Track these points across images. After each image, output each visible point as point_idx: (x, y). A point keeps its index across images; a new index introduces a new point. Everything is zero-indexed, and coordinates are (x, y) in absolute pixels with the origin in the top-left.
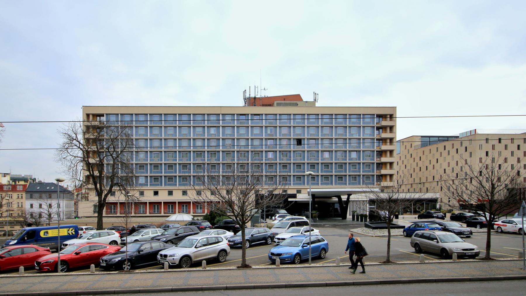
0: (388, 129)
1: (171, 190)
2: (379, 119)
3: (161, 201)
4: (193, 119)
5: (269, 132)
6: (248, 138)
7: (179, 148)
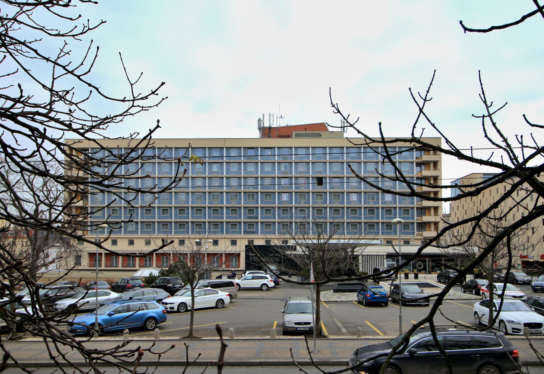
0: (432, 166)
2: (421, 153)
4: (312, 152)
5: (283, 169)
6: (256, 176)
7: (209, 189)
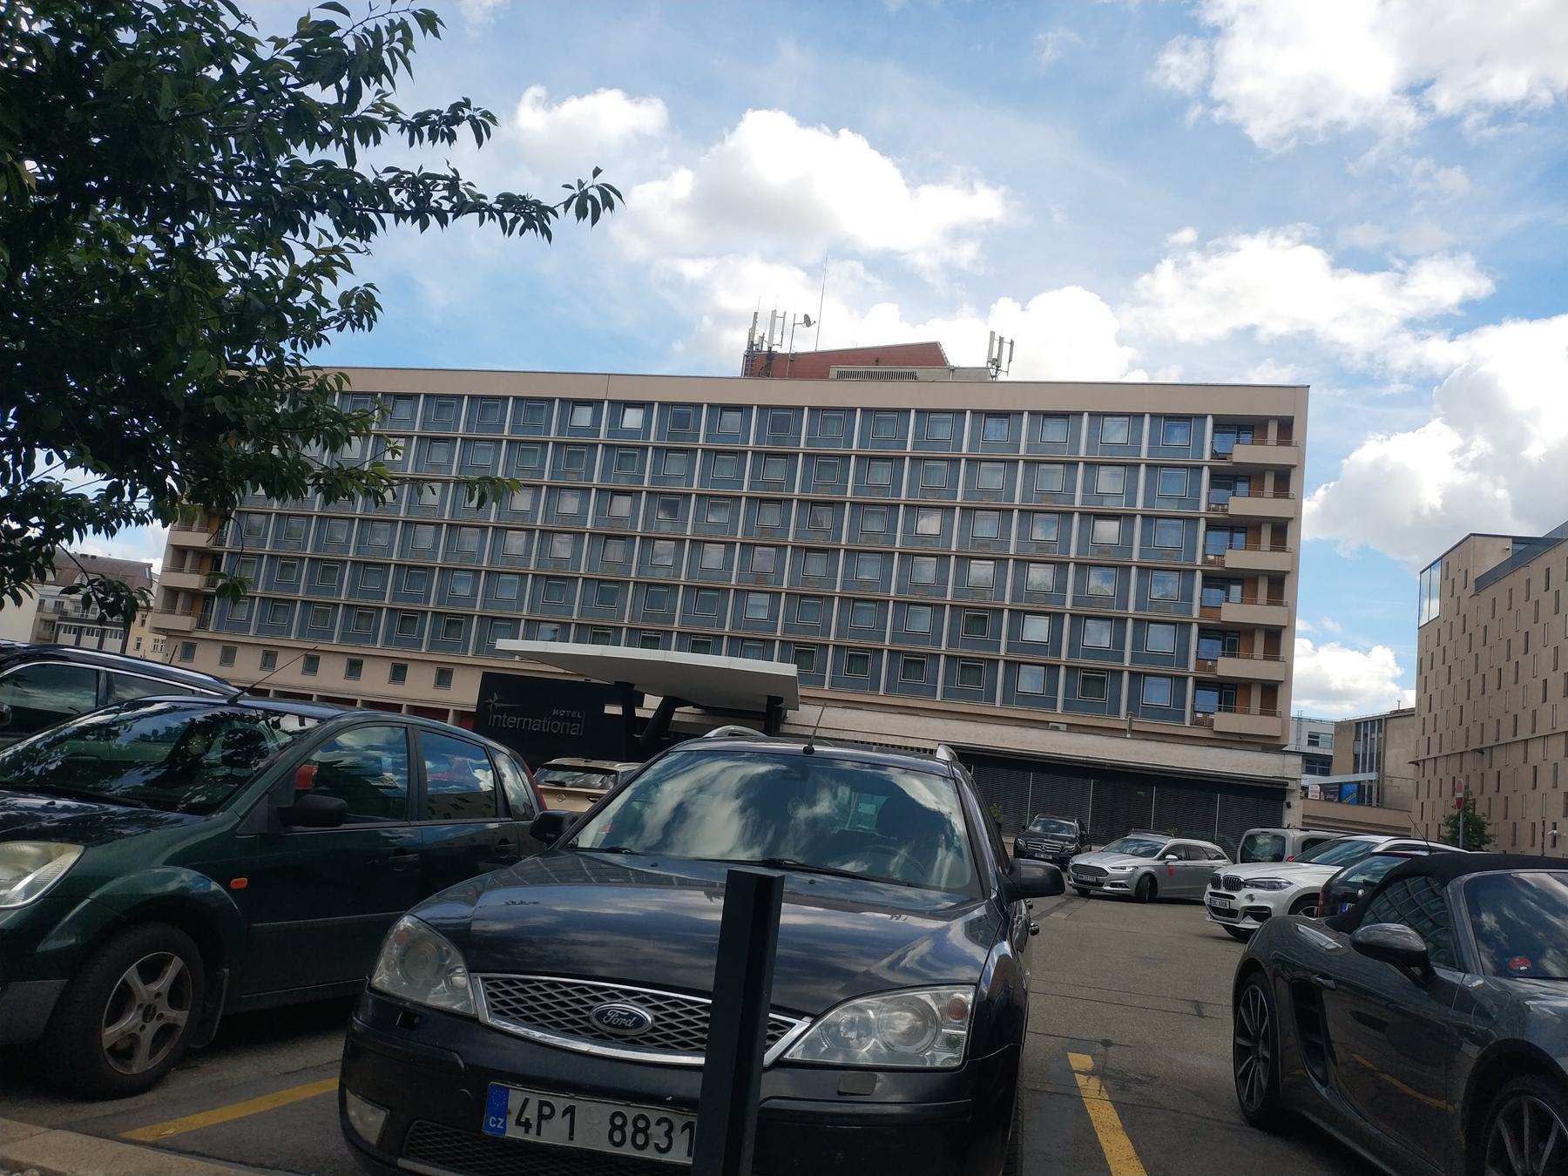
0: (1266, 535)
1: (358, 658)
3: (448, 708)
